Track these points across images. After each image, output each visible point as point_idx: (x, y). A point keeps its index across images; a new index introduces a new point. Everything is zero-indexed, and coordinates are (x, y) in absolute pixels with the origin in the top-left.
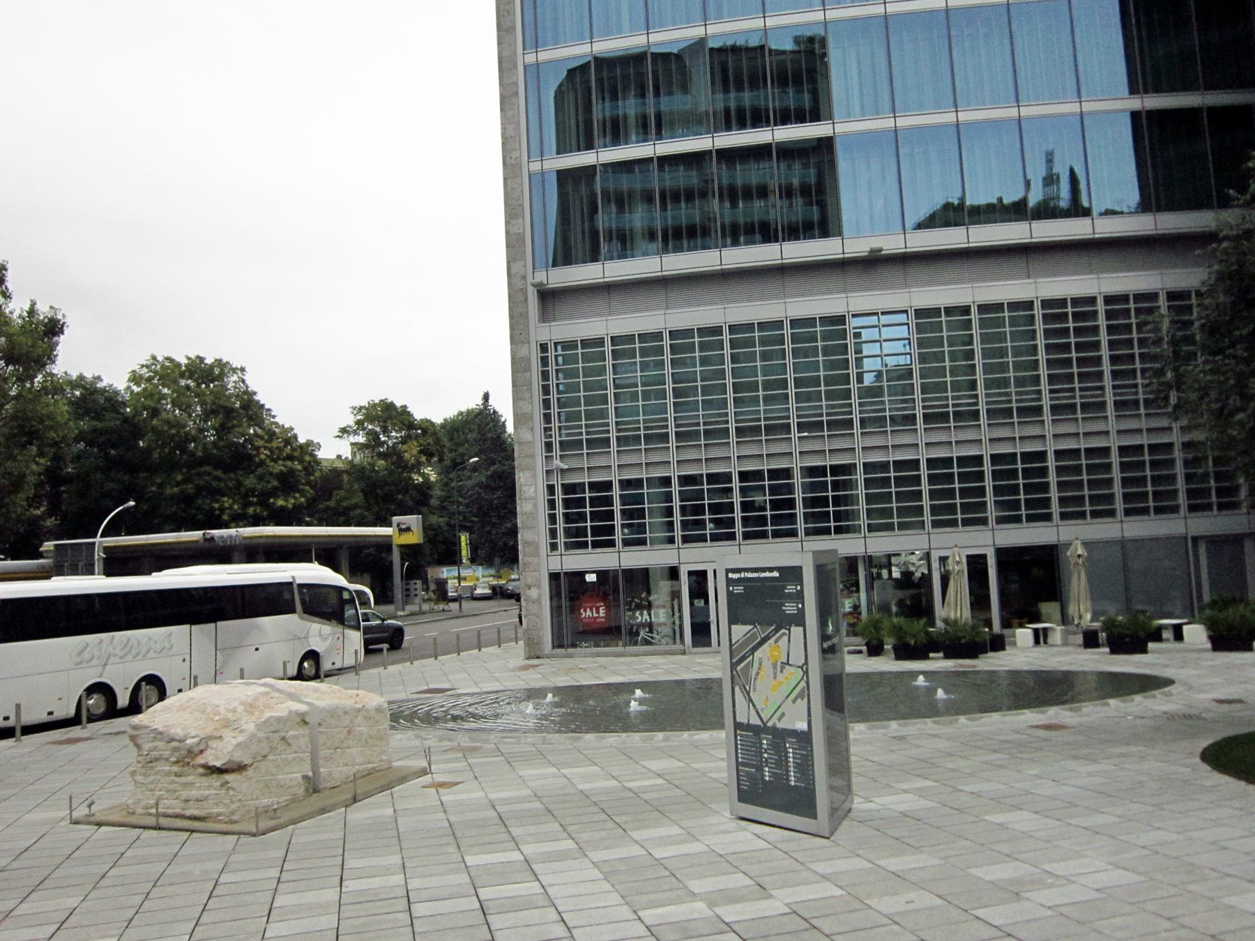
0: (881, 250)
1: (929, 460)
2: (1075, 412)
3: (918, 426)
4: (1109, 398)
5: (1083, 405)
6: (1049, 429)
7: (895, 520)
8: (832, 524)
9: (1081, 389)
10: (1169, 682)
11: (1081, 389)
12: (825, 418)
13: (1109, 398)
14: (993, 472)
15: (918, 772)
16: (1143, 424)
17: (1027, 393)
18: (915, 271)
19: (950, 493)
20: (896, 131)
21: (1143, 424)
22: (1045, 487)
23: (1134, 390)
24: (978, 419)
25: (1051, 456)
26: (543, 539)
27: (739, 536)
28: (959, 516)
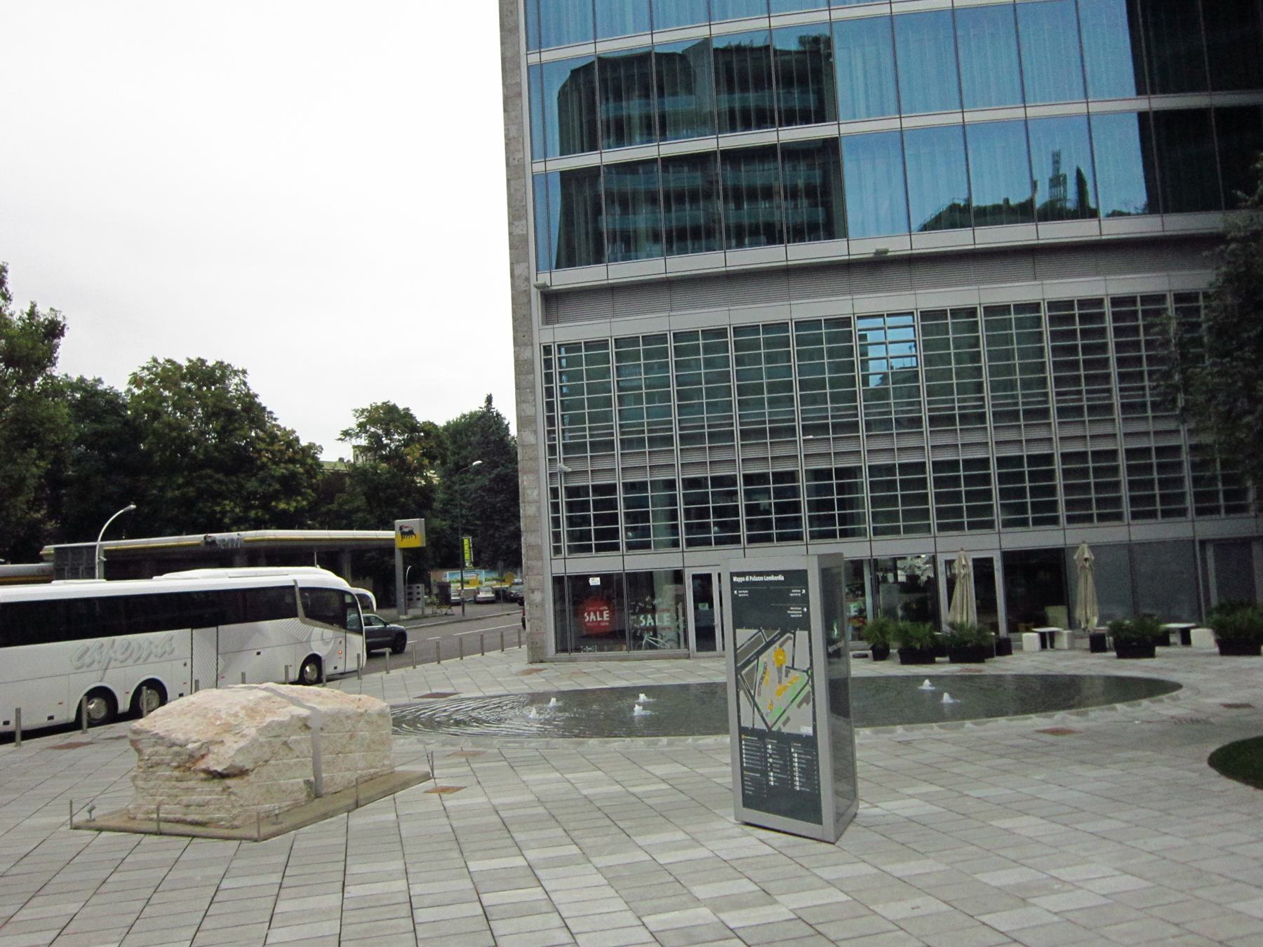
0: (886, 251)
2: (1081, 415)
4: (1116, 400)
5: (1090, 407)
6: (1056, 432)
7: (901, 524)
9: (1088, 392)
12: (830, 421)
13: (1116, 400)
16: (1150, 426)
21: (1150, 426)
22: (1052, 490)
24: (984, 422)
25: (1057, 459)
26: (547, 543)
27: (744, 539)
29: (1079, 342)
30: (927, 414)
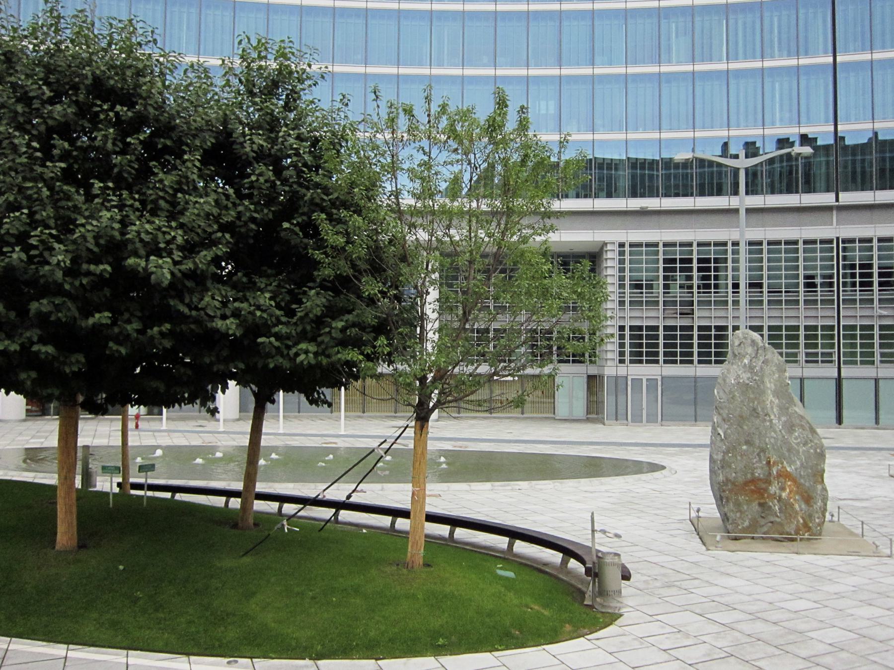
0: (647, 207)
1: (664, 326)
3: (875, 306)
4: (802, 298)
6: (766, 313)
8: (644, 358)
9: (821, 291)
10: (663, 468)
11: (860, 291)
12: (644, 299)
13: (802, 298)
14: (769, 335)
15: (528, 512)
17: (684, 293)
18: (768, 217)
19: (674, 346)
20: (660, 140)
22: (657, 345)
23: (871, 293)
24: (762, 305)
25: (802, 329)
28: (859, 359)
29: (819, 263)
30: (878, 297)
